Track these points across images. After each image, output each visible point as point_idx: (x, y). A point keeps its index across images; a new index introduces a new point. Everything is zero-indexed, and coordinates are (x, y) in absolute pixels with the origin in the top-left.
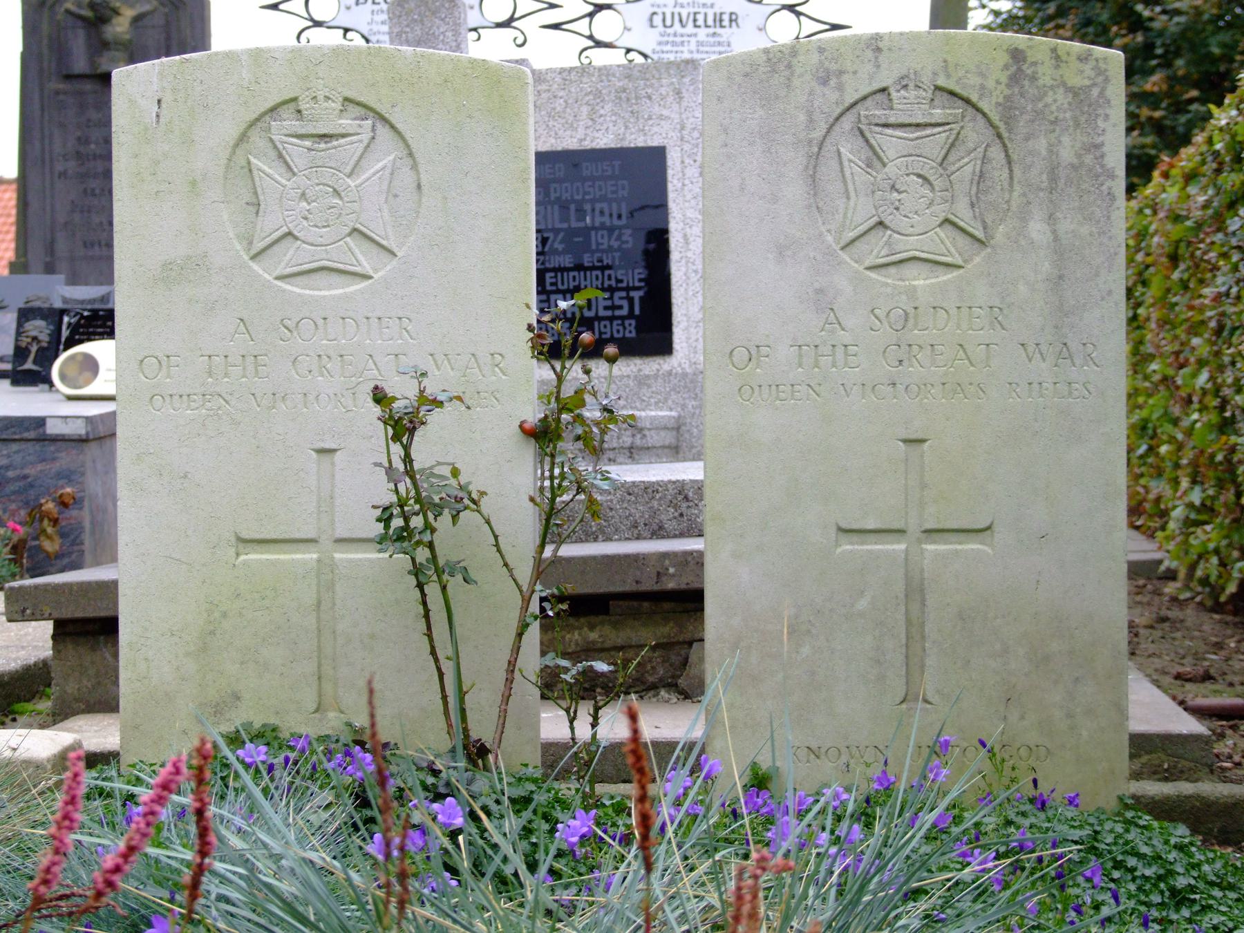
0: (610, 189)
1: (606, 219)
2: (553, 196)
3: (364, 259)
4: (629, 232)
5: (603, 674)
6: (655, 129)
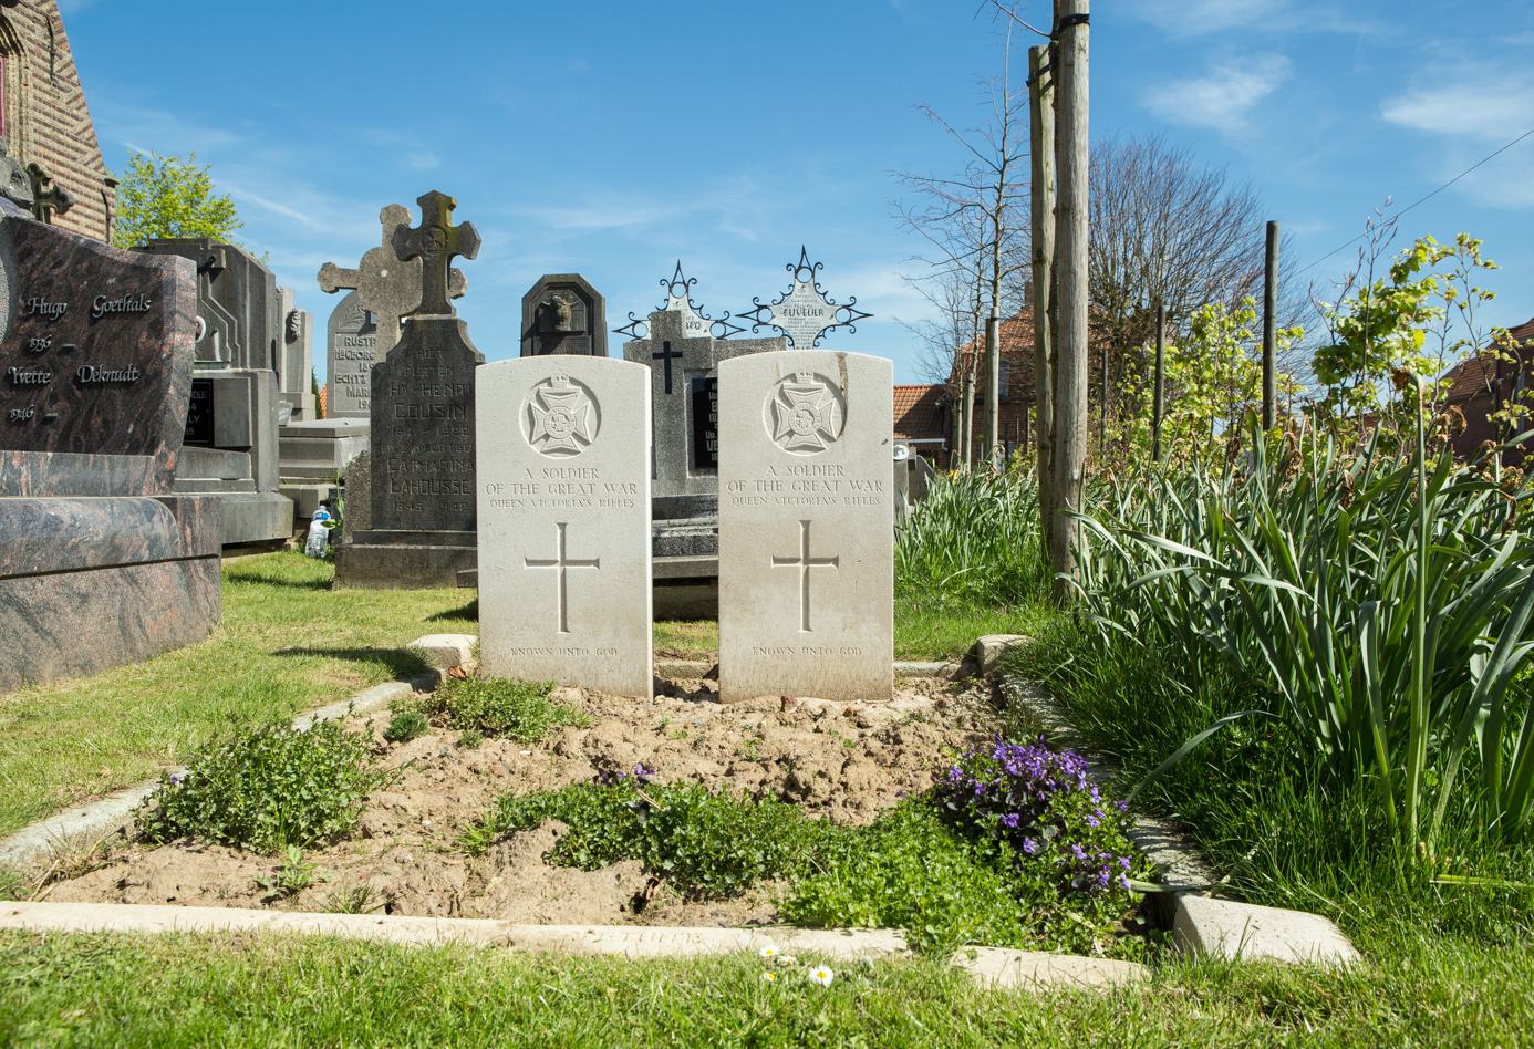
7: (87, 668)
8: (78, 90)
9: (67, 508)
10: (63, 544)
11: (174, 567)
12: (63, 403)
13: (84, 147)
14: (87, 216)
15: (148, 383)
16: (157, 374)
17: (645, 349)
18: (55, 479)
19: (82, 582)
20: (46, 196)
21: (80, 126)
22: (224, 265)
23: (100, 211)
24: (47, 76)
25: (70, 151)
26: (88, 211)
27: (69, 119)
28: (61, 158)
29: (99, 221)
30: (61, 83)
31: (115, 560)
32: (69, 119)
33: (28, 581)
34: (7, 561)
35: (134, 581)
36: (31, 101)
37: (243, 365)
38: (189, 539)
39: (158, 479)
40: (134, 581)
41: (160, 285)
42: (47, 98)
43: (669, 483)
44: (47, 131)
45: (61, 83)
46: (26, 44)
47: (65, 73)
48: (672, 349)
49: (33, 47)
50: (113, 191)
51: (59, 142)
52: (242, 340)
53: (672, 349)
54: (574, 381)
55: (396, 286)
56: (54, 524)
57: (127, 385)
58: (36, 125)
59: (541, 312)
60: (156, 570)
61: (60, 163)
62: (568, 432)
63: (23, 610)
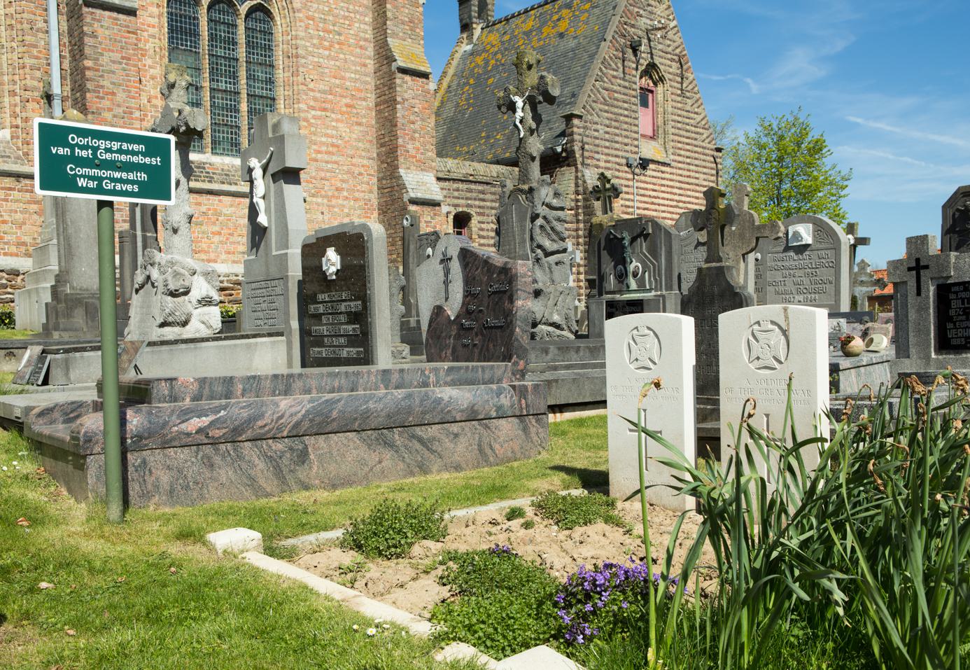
7: (458, 468)
8: (698, 96)
9: (447, 393)
10: (442, 411)
11: (515, 420)
12: (480, 337)
13: (701, 131)
14: (704, 173)
15: (508, 326)
16: (511, 321)
17: (902, 264)
18: (449, 379)
19: (455, 428)
20: (609, 189)
21: (699, 118)
22: (650, 231)
23: (712, 169)
24: (679, 92)
25: (693, 135)
26: (705, 170)
27: (692, 115)
28: (688, 141)
29: (712, 175)
30: (688, 94)
31: (473, 416)
32: (692, 115)
33: (423, 428)
34: (411, 419)
35: (487, 427)
36: (670, 109)
37: (661, 290)
38: (524, 406)
39: (513, 374)
40: (487, 427)
41: (512, 277)
42: (680, 105)
43: (919, 361)
44: (679, 125)
45: (688, 94)
46: (667, 76)
47: (690, 87)
48: (922, 264)
49: (671, 77)
50: (720, 154)
51: (687, 131)
52: (660, 275)
53: (922, 264)
54: (649, 328)
55: (740, 235)
56: (439, 401)
57: (502, 327)
58: (673, 123)
59: (957, 214)
60: (503, 422)
61: (688, 144)
62: (646, 357)
63: (420, 440)
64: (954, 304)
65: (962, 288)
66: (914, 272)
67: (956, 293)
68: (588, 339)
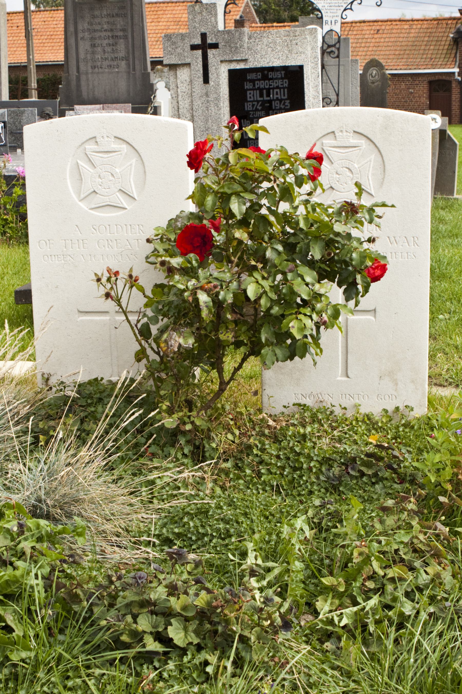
0: (280, 83)
1: (279, 96)
2: (256, 87)
3: (123, 201)
4: (288, 101)
5: (260, 339)
6: (299, 58)
48: (209, 41)
53: (209, 41)
64: (250, 95)
65: (259, 75)
66: (200, 52)
67: (253, 81)
68: (279, 202)
